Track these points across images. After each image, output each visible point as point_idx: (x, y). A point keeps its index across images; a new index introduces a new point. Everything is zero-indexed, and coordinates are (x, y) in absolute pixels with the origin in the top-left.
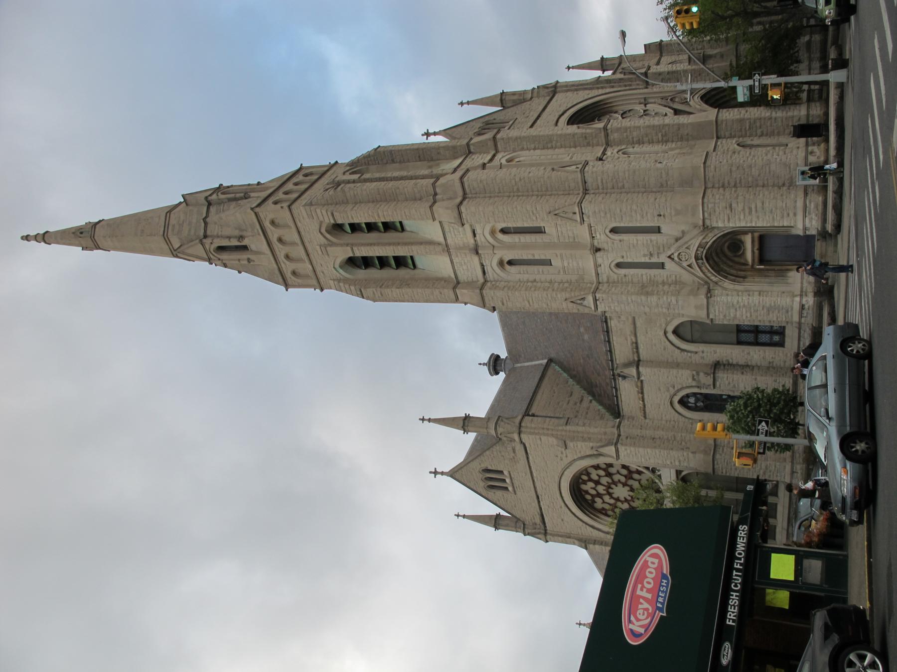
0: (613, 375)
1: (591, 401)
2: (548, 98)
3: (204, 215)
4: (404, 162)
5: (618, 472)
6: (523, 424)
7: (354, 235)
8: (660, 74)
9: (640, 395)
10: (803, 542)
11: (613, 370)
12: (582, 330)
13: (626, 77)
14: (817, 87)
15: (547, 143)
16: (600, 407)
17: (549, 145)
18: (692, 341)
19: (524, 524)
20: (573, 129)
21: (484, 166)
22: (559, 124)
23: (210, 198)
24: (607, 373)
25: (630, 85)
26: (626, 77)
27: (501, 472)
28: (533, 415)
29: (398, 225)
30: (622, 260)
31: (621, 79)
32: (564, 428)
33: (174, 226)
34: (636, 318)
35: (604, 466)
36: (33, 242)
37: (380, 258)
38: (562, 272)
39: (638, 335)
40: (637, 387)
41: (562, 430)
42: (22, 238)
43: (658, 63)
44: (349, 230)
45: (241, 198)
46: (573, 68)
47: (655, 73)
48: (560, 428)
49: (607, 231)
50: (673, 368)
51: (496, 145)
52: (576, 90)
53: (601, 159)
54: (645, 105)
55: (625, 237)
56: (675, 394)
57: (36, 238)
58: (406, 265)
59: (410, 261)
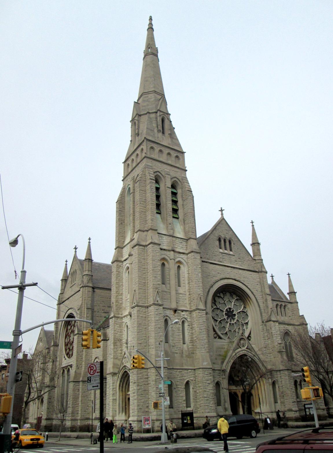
3: (150, 112)
6: (87, 288)
10: (67, 421)
14: (189, 422)
16: (102, 322)
17: (190, 281)
19: (63, 293)
28: (94, 291)
32: (85, 308)
36: (148, 22)
38: (126, 299)
41: (84, 307)
42: (151, 17)
46: (289, 277)
48: (86, 306)
50: (103, 357)
57: (151, 24)
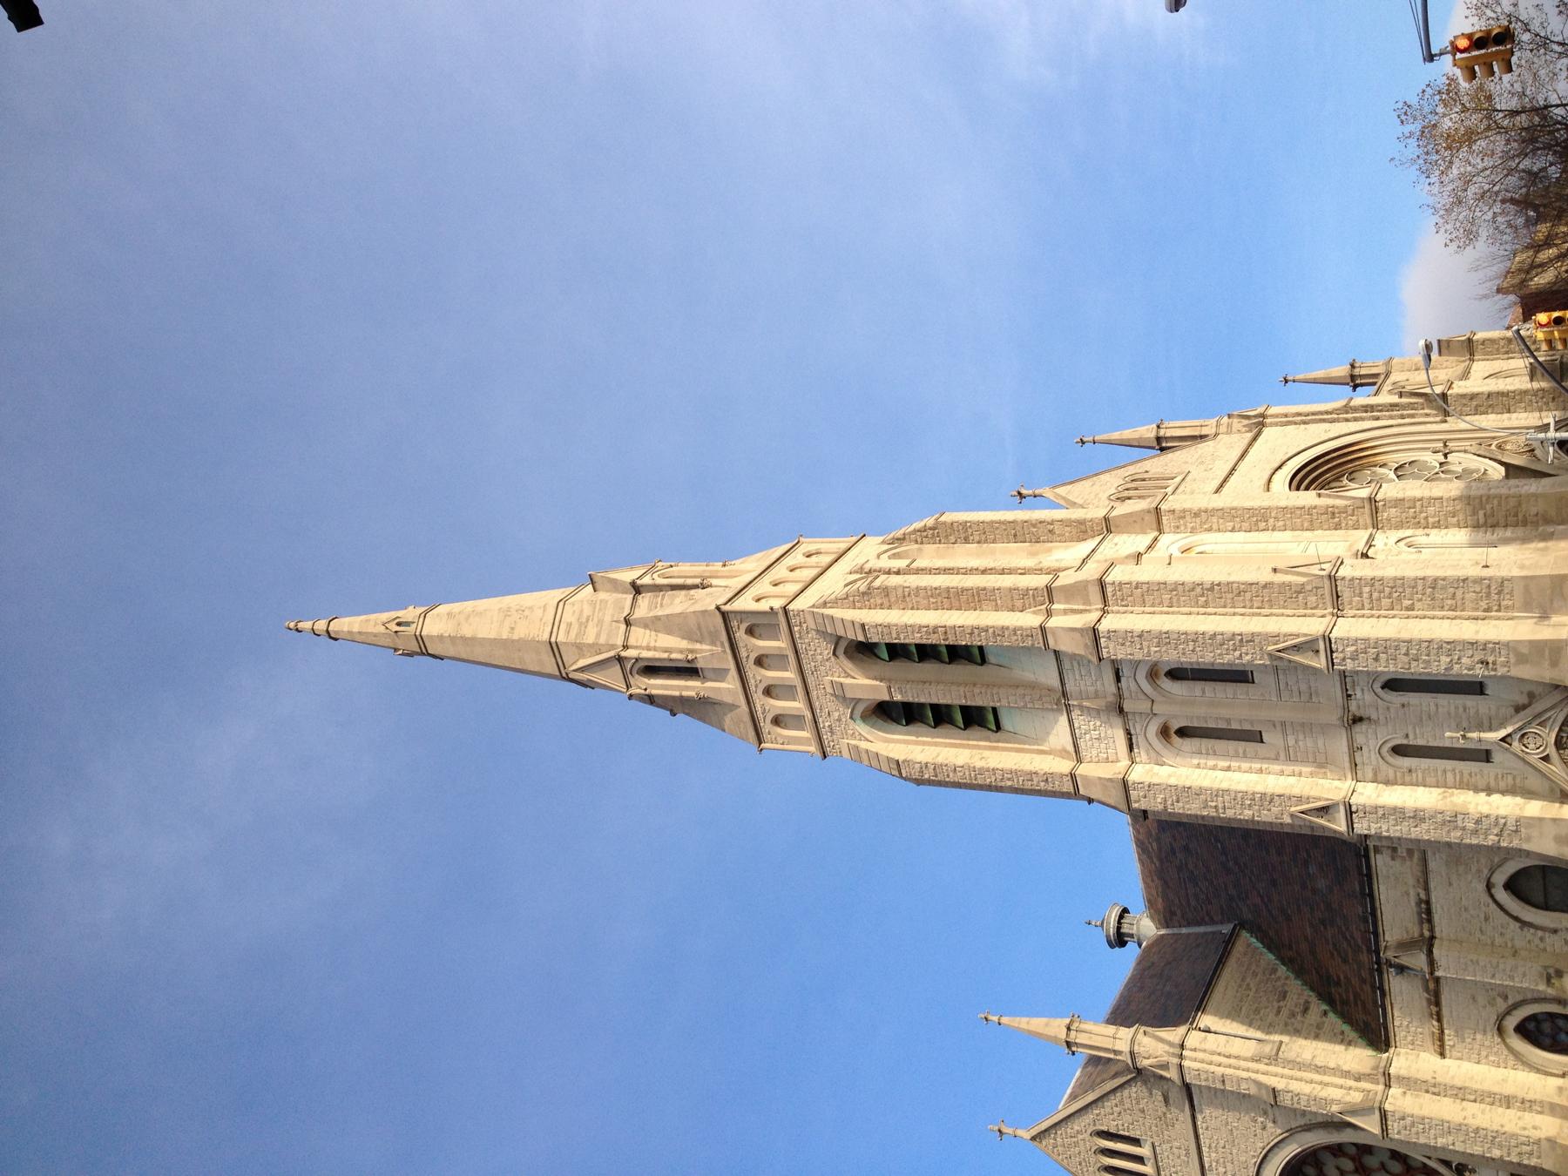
0: (1378, 962)
1: (1325, 1013)
2: (1250, 436)
4: (986, 541)
5: (1383, 1166)
7: (952, 667)
8: (1473, 396)
9: (1434, 1009)
11: (1377, 952)
12: (1312, 869)
13: (1405, 400)
15: (1257, 519)
18: (1546, 907)
20: (1308, 498)
21: (1139, 556)
22: (1272, 485)
23: (639, 582)
24: (1364, 957)
25: (1412, 416)
26: (1405, 400)
27: (1136, 1142)
29: (976, 652)
30: (1405, 742)
31: (1393, 406)
33: (570, 625)
34: (1429, 854)
35: (1353, 1151)
37: (936, 708)
39: (1432, 885)
40: (1427, 990)
43: (1465, 375)
44: (885, 655)
45: (696, 587)
47: (1463, 396)
49: (1377, 686)
51: (1159, 522)
52: (1305, 423)
53: (1365, 556)
54: (1445, 456)
55: (1413, 698)
56: (1508, 1012)
58: (982, 723)
59: (991, 717)
